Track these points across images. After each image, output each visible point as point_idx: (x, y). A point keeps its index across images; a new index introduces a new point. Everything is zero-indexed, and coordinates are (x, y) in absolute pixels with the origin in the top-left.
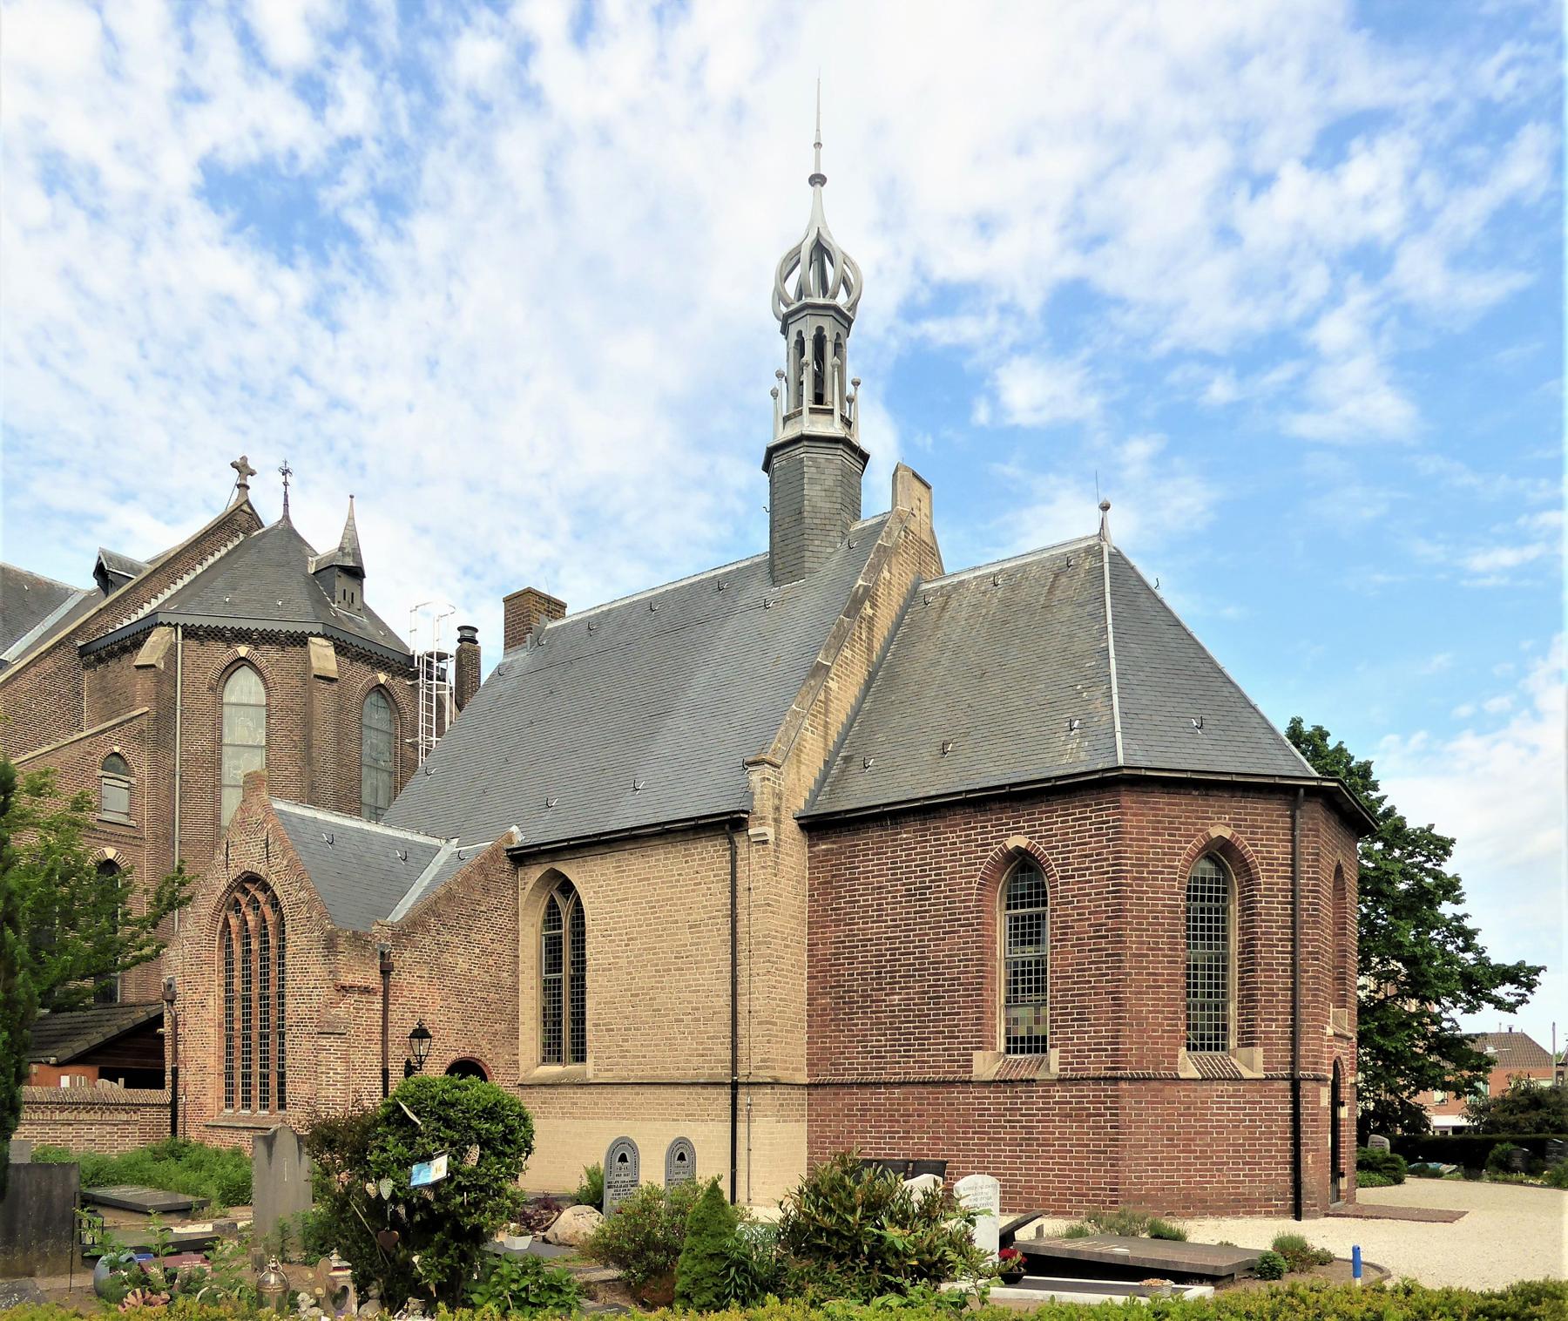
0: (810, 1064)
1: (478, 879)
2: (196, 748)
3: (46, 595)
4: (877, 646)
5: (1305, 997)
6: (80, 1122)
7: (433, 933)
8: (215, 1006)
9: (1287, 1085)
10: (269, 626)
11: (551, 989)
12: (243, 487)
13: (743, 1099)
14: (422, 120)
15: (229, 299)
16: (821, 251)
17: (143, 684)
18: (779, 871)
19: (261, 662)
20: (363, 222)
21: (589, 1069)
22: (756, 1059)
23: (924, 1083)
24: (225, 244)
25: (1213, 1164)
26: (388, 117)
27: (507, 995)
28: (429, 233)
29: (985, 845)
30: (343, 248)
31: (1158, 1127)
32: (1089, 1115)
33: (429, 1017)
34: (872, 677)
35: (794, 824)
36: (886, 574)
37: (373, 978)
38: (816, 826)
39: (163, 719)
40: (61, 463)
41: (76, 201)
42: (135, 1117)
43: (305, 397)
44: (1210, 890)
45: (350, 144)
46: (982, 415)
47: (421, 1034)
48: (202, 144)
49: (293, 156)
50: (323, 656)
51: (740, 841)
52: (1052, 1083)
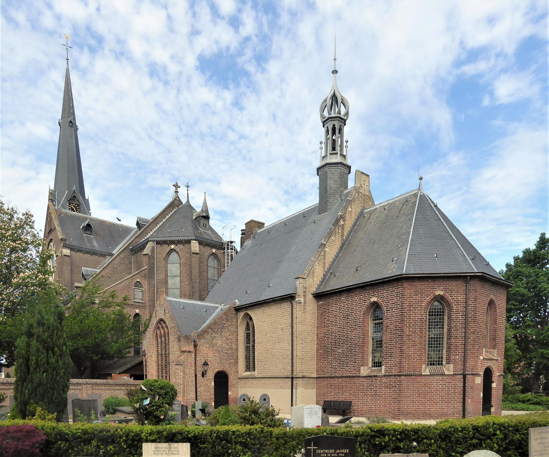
3: (126, 230)
4: (345, 234)
5: (469, 347)
8: (154, 358)
9: (462, 376)
10: (179, 238)
11: (247, 349)
12: (177, 192)
13: (295, 382)
14: (273, 25)
15: (207, 105)
16: (334, 98)
17: (145, 260)
18: (307, 311)
20: (251, 68)
21: (256, 373)
22: (298, 370)
23: (347, 377)
24: (206, 85)
26: (260, 26)
27: (234, 351)
30: (244, 79)
34: (343, 244)
35: (312, 296)
36: (350, 209)
37: (192, 348)
38: (318, 296)
39: (151, 270)
40: (155, 171)
41: (160, 79)
43: (232, 136)
44: (438, 312)
45: (247, 39)
46: (486, 102)
47: (206, 364)
48: (198, 50)
49: (228, 48)
50: (195, 246)
51: (294, 302)
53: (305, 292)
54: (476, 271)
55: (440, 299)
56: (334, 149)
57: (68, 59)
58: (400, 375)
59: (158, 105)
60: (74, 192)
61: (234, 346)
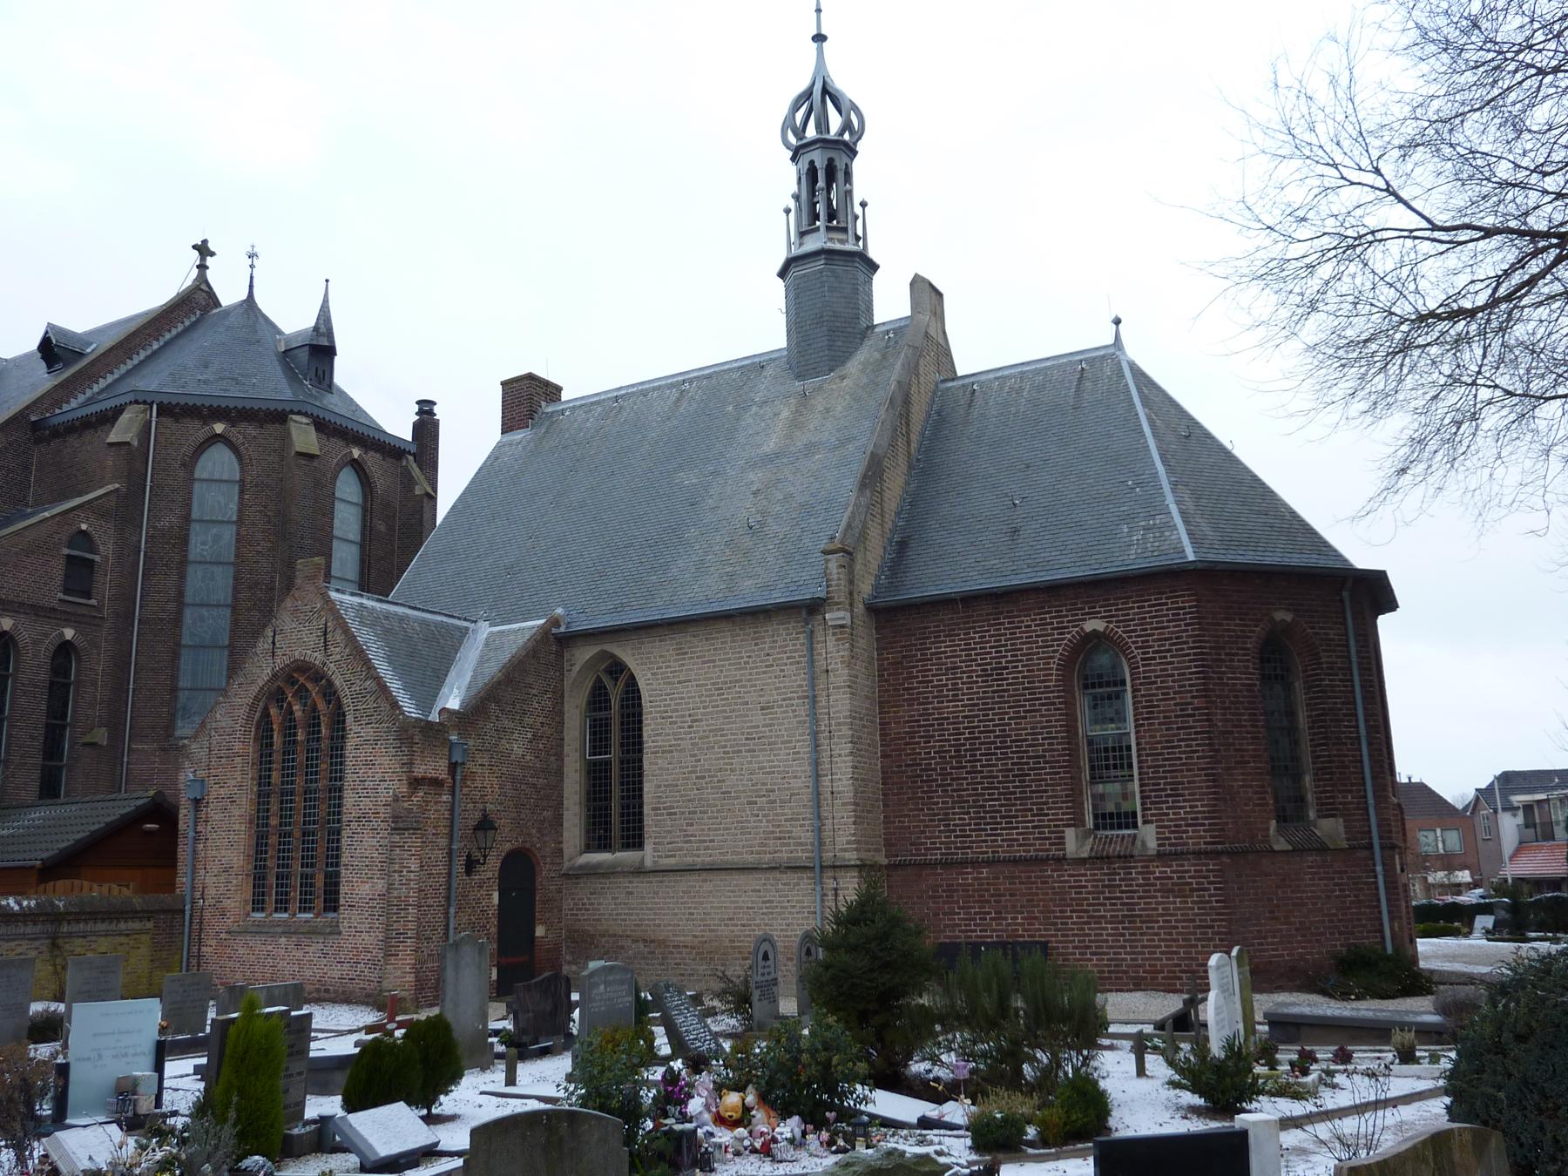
0: (888, 844)
2: (165, 523)
6: (94, 933)
12: (202, 267)
19: (238, 440)
21: (648, 855)
29: (1061, 629)
32: (1192, 890)
33: (489, 807)
42: (150, 925)
50: (304, 437)
52: (1151, 859)
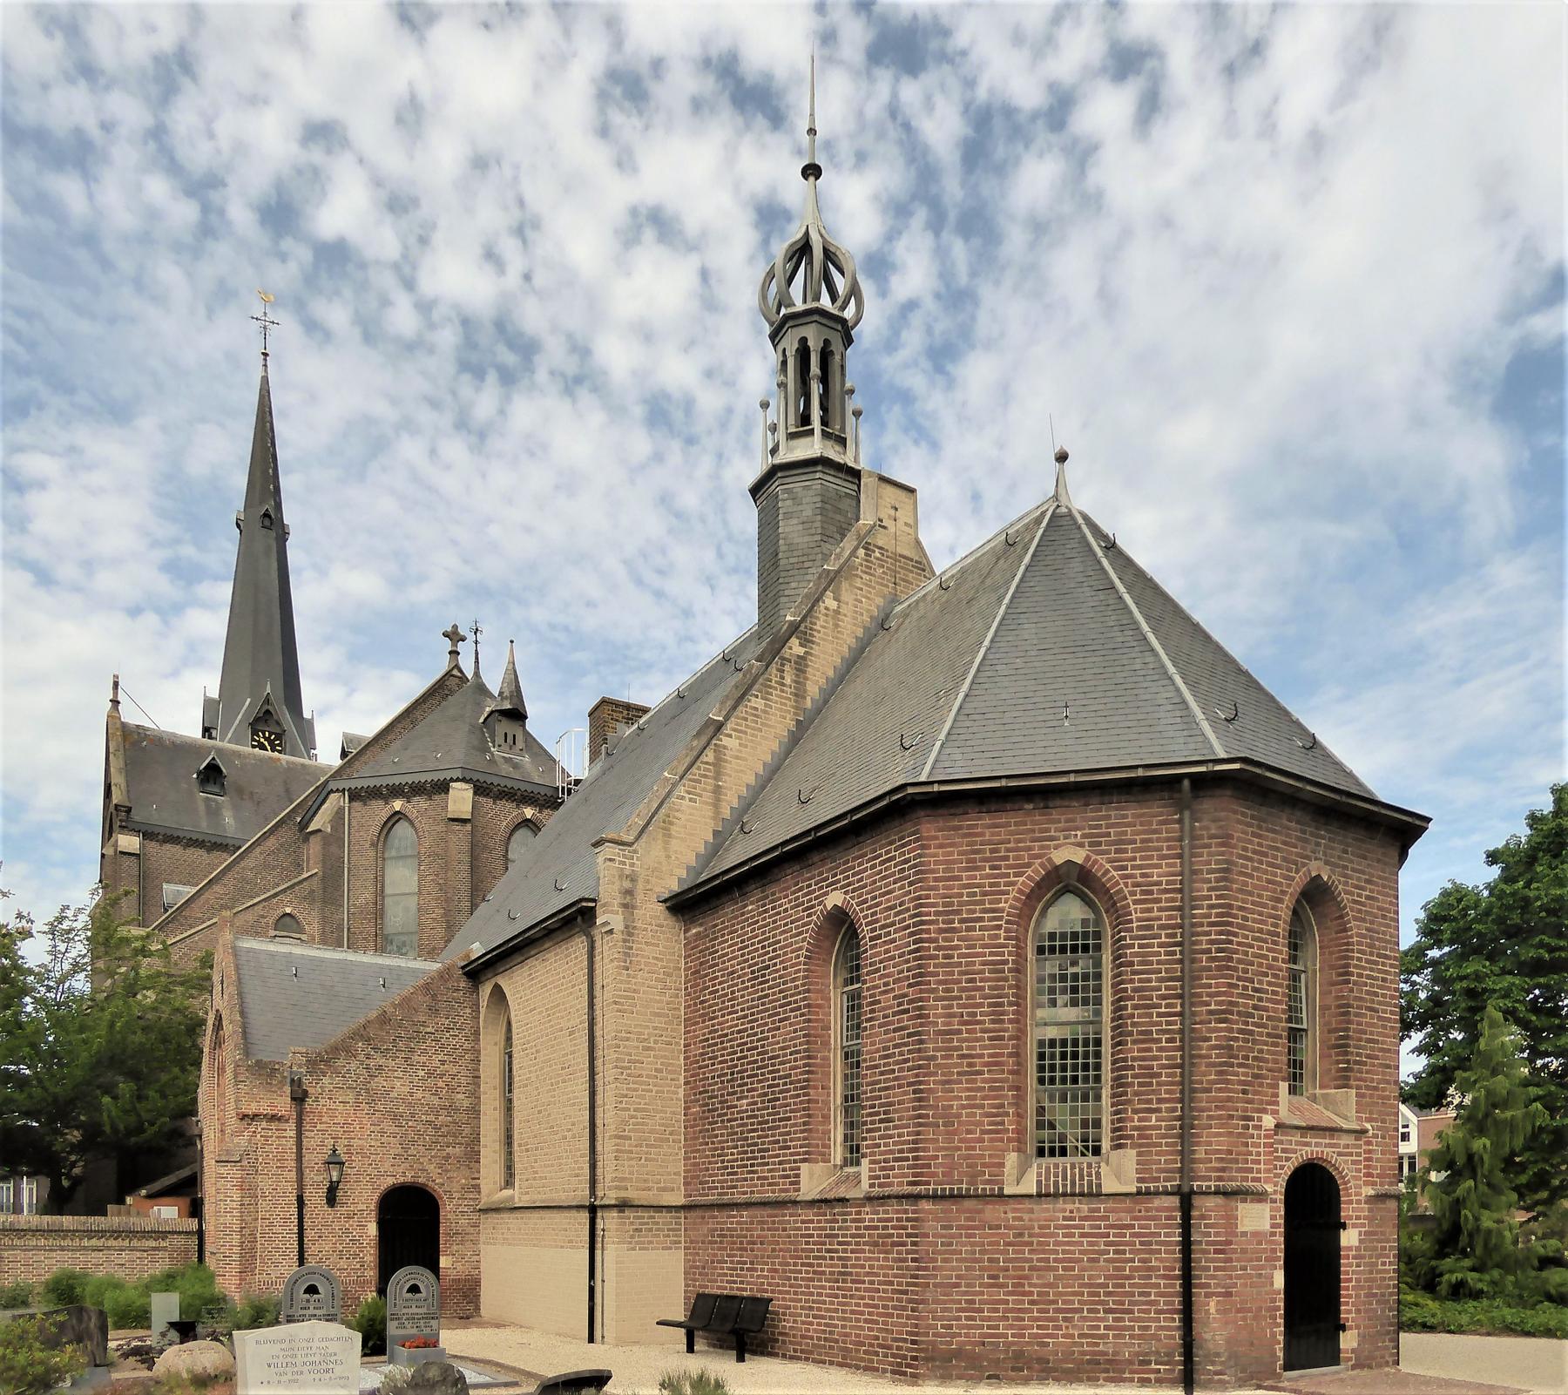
1: (423, 1001)
2: (362, 901)
5: (1206, 1076)
6: (109, 1248)
7: (362, 1057)
9: (1175, 1201)
10: (416, 778)
12: (454, 653)
20: (916, 381)
22: (609, 1177)
25: (1057, 1311)
28: (978, 372)
30: (897, 408)
31: (976, 1261)
35: (662, 907)
38: (690, 905)
42: (163, 1244)
45: (910, 306)
47: (334, 1161)
50: (461, 799)
53: (629, 892)
54: (1223, 755)
55: (1073, 881)
56: (805, 419)
57: (265, 355)
58: (917, 1197)
59: (665, 500)
60: (267, 701)
61: (462, 1100)
